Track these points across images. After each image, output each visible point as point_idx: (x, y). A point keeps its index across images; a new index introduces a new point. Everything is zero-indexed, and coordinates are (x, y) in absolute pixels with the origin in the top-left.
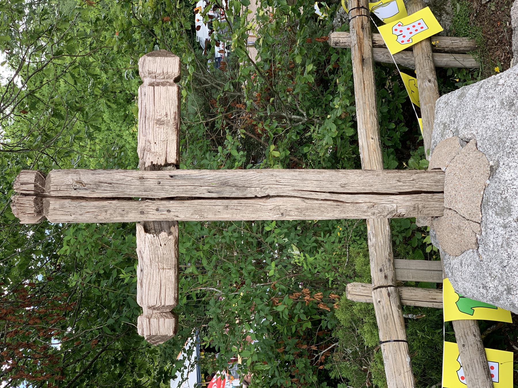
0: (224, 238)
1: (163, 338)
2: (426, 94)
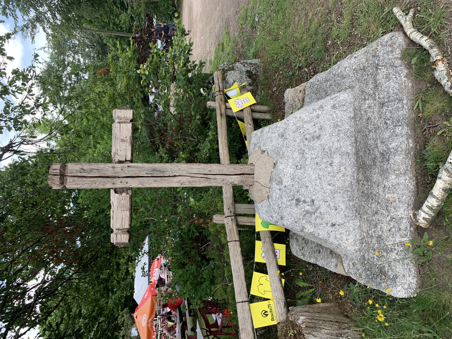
0: (158, 194)
1: (123, 244)
2: (249, 130)
